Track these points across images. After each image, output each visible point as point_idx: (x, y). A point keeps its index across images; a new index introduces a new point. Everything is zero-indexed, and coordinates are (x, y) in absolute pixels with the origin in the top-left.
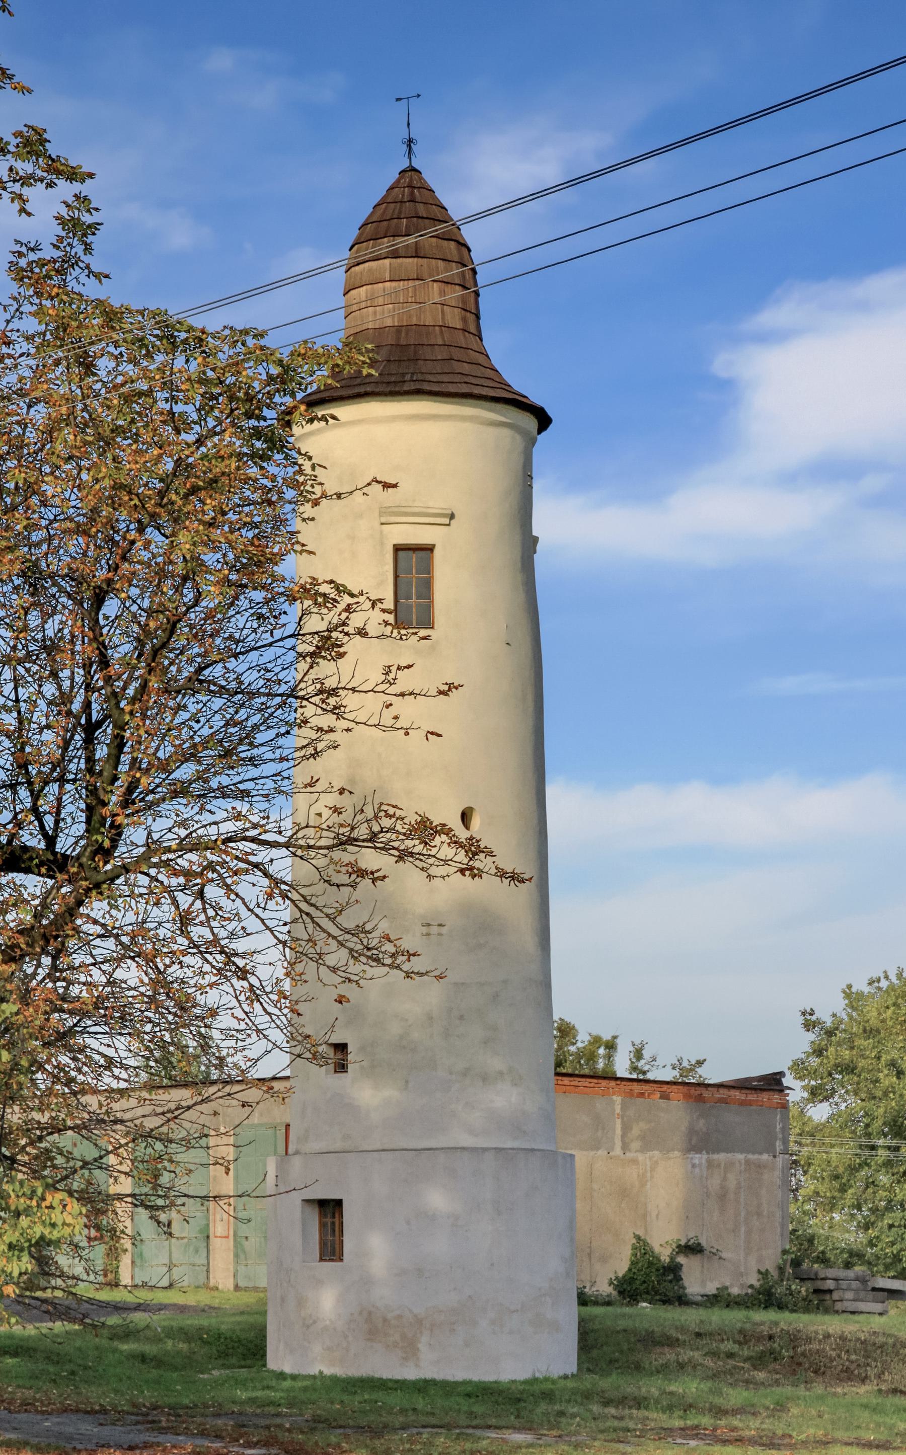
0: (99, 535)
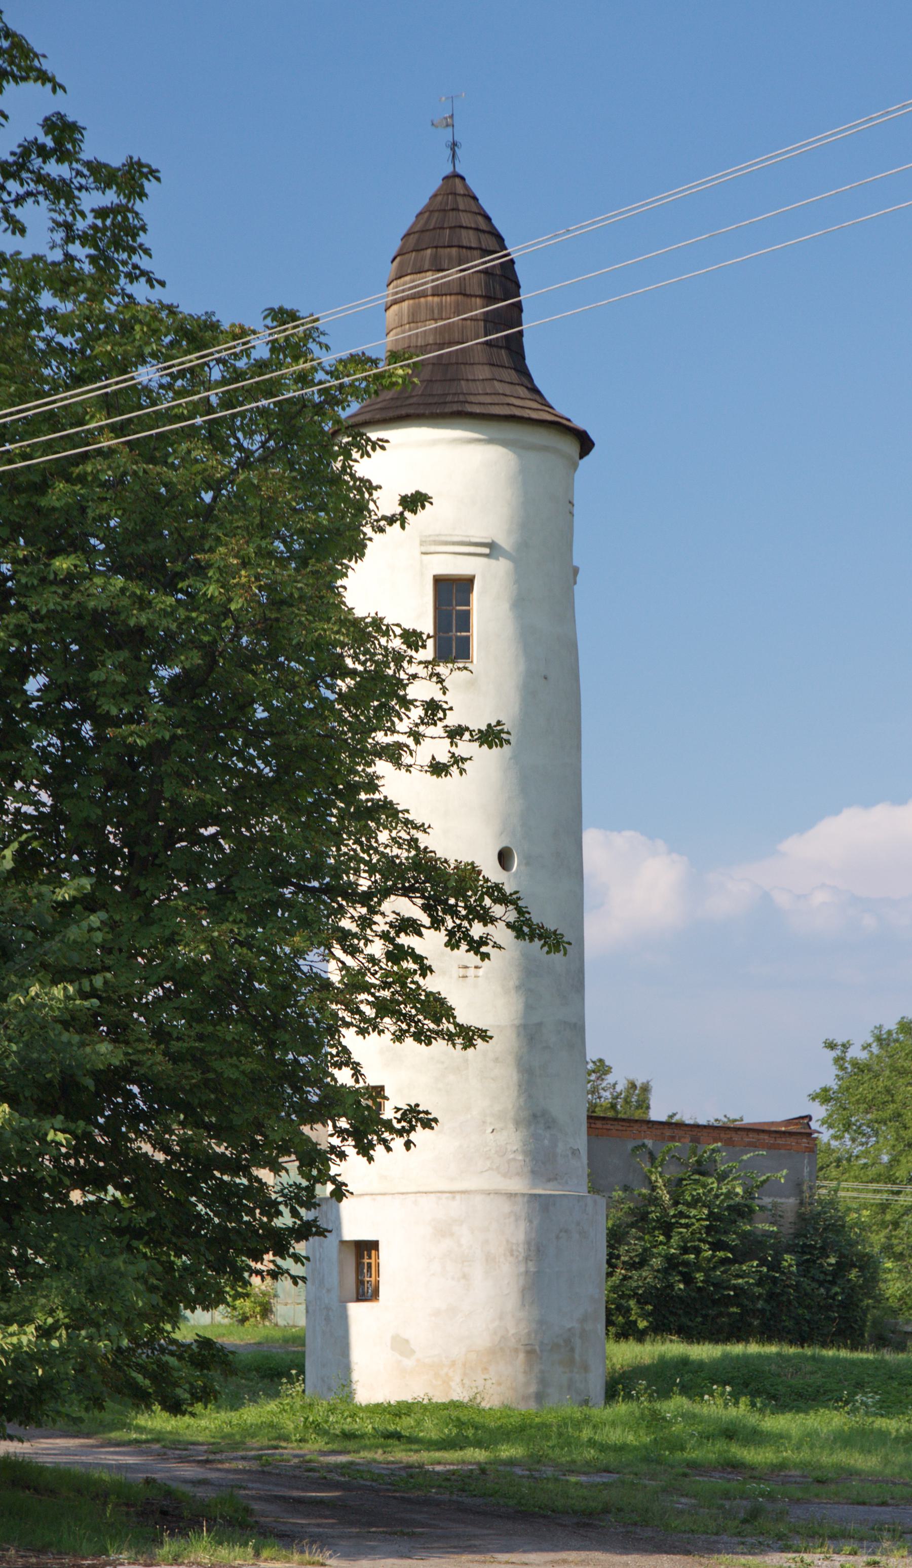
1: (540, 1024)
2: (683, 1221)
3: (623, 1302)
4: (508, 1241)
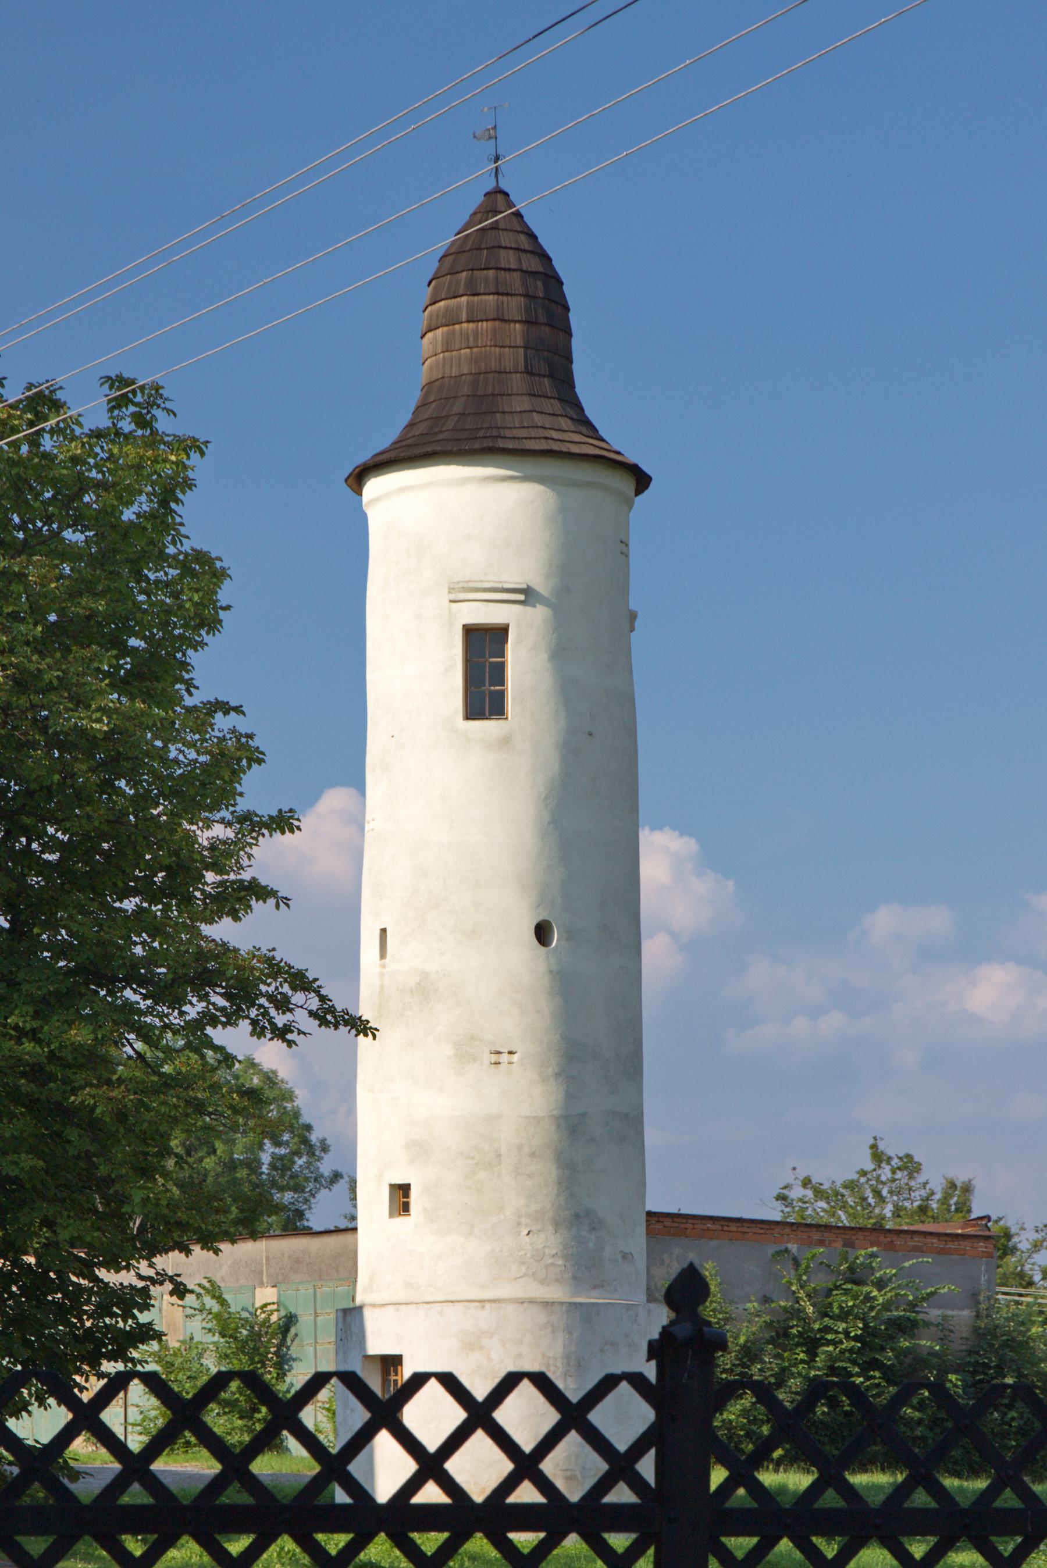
1: (584, 1115)
2: (829, 1337)
3: (754, 1427)
4: (543, 1355)
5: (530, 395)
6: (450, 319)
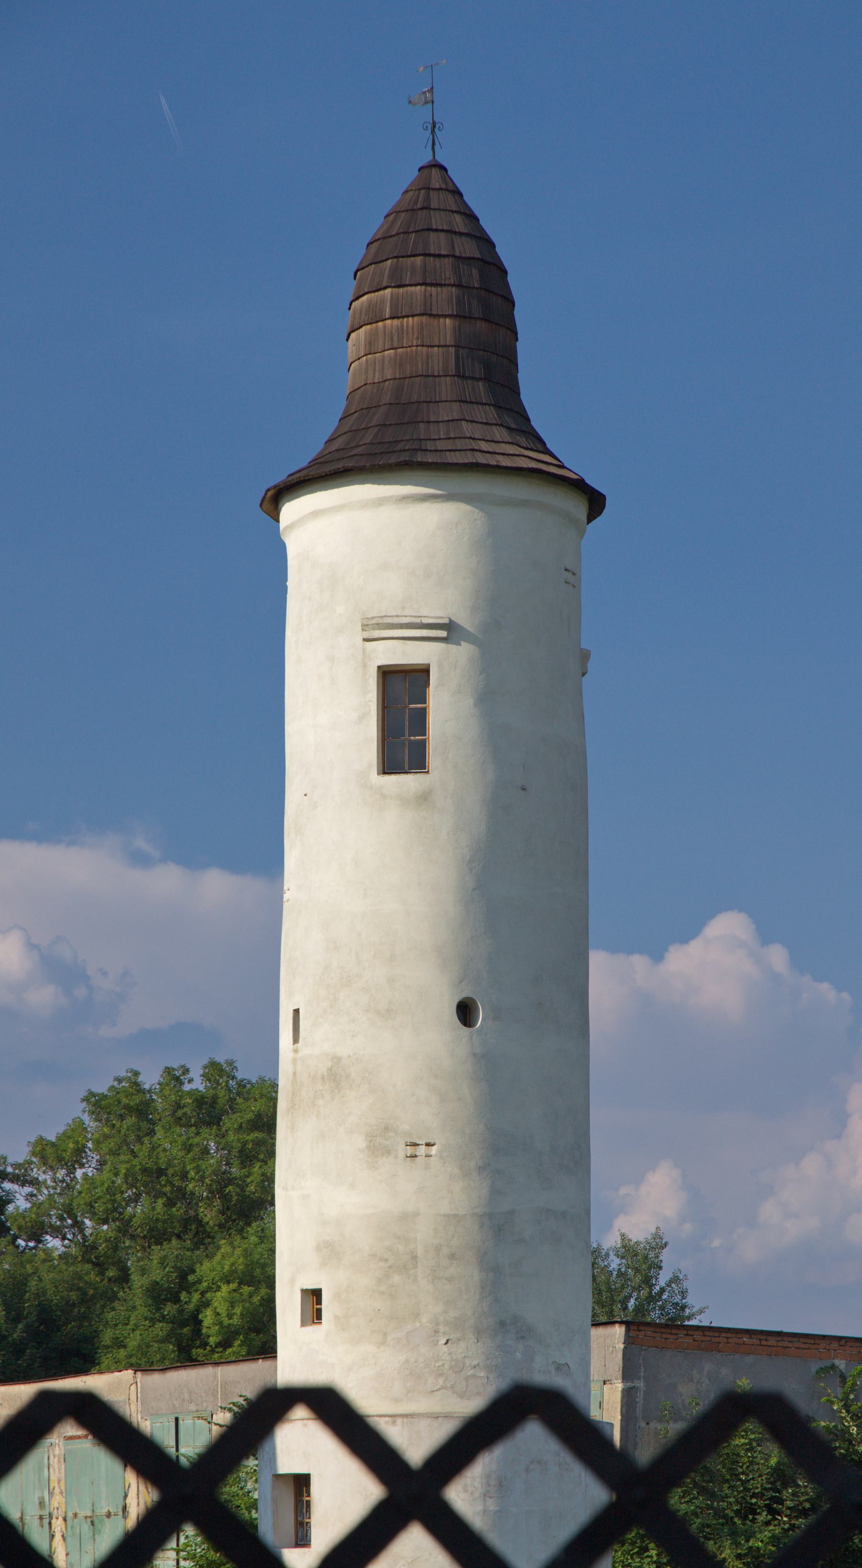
0: (163, 1183)
1: (512, 1212)
5: (459, 401)
6: (374, 317)
